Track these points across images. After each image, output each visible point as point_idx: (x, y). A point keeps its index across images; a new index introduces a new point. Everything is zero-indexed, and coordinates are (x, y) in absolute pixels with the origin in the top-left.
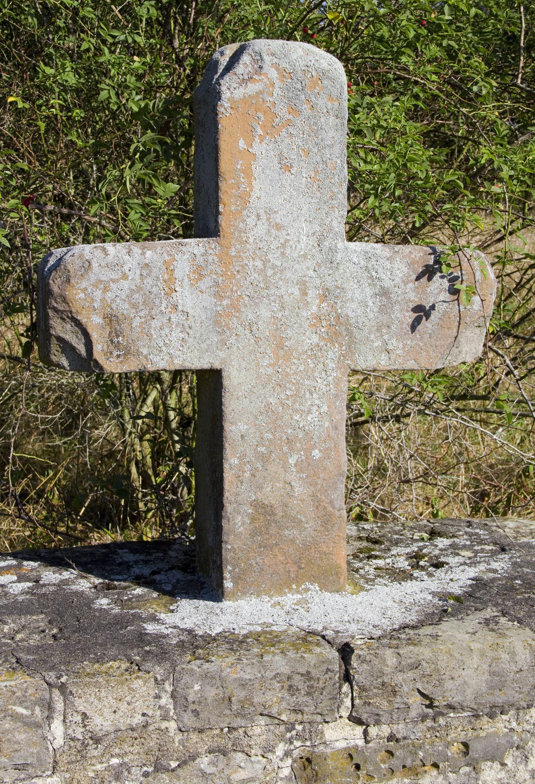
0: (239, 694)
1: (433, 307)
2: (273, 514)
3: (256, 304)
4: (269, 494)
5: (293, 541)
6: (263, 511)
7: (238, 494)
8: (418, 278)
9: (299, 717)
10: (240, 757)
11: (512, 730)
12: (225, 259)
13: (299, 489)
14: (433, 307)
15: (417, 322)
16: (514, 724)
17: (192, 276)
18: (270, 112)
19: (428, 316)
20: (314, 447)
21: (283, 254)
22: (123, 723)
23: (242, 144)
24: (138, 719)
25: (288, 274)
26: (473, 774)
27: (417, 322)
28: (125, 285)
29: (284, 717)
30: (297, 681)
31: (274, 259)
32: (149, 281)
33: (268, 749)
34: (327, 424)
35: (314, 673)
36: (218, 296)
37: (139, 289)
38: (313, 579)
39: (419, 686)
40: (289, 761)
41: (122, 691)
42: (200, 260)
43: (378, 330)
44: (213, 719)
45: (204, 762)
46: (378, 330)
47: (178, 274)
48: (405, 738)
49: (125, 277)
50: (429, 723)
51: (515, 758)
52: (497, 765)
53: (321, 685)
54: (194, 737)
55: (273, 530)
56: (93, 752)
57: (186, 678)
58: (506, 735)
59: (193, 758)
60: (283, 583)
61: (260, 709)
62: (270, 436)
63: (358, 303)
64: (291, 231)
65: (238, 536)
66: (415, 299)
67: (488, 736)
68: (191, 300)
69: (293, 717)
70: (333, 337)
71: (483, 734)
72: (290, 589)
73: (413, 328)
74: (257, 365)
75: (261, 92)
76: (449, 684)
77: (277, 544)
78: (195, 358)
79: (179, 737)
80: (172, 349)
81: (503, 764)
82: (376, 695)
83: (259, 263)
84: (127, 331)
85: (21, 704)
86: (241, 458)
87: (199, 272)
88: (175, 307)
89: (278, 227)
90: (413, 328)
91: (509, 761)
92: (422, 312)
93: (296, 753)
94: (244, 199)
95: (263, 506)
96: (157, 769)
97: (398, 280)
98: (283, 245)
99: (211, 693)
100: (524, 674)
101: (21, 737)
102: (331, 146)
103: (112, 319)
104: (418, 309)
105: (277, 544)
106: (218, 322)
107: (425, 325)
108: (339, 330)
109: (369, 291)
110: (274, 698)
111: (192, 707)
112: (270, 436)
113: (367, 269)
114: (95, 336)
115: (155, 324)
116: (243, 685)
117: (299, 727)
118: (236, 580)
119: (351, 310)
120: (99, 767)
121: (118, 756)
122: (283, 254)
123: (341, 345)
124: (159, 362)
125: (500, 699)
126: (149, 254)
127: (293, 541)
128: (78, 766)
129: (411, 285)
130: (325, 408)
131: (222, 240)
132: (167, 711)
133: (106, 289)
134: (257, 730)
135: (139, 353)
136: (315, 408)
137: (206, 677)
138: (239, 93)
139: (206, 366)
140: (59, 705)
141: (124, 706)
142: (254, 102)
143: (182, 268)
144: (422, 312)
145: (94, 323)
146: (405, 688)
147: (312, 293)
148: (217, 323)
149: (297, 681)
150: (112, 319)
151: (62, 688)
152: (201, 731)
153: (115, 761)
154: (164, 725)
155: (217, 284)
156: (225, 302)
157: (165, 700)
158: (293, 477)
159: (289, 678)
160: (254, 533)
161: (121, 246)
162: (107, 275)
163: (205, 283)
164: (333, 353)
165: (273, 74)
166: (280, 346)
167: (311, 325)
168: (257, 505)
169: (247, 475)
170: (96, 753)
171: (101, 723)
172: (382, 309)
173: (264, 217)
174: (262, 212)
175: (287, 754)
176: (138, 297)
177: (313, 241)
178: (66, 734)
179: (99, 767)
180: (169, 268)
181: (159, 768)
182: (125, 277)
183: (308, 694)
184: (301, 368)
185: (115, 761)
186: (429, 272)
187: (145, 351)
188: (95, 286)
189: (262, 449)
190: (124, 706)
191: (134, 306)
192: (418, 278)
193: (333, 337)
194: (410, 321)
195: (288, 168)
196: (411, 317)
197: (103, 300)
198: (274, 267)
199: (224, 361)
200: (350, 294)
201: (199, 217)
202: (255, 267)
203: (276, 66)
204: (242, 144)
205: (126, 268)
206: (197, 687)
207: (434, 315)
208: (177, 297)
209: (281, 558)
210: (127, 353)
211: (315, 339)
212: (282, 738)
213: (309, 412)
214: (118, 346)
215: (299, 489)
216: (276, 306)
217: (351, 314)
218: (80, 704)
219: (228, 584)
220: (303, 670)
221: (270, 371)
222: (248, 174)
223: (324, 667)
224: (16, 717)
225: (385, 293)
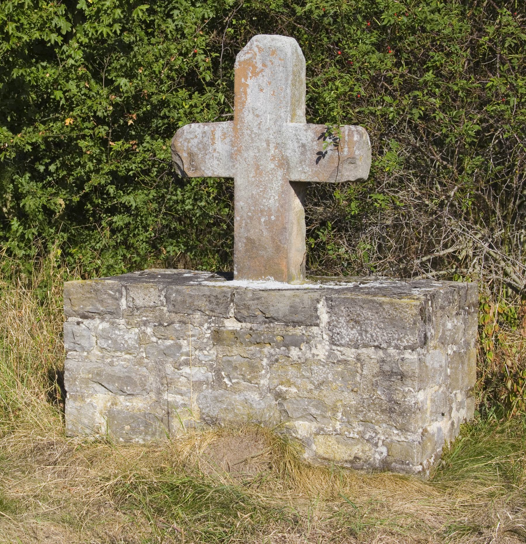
0: (189, 300)
1: (326, 152)
2: (254, 243)
3: (248, 150)
4: (253, 234)
5: (263, 256)
6: (250, 241)
7: (239, 233)
8: (319, 139)
9: (214, 314)
10: (190, 326)
11: (303, 334)
12: (235, 129)
13: (265, 233)
14: (326, 152)
15: (318, 159)
16: (304, 332)
17: (222, 137)
18: (254, 67)
19: (324, 156)
20: (272, 215)
21: (259, 128)
22: (146, 304)
23: (243, 80)
24: (152, 304)
25: (261, 137)
26: (287, 351)
27: (318, 159)
28: (196, 140)
29: (207, 313)
30: (212, 298)
31: (255, 130)
32: (205, 139)
33: (201, 325)
34: (278, 205)
35: (219, 296)
36: (232, 146)
37: (202, 142)
38: (272, 275)
39: (259, 307)
40: (209, 331)
41: (146, 292)
42: (225, 130)
43: (300, 163)
44: (180, 309)
45: (177, 326)
46: (300, 163)
47: (216, 136)
48: (257, 330)
49: (196, 137)
50: (267, 325)
51: (306, 347)
52: (297, 349)
53: (221, 301)
54: (173, 315)
55: (255, 251)
56: (136, 313)
57: (170, 291)
58: (300, 336)
59: (173, 323)
60: (258, 275)
61: (197, 308)
62: (253, 208)
63: (292, 152)
64: (263, 118)
65: (240, 251)
66: (317, 149)
67: (293, 335)
68: (221, 147)
69: (211, 313)
70: (281, 165)
71: (290, 334)
72: (262, 278)
73: (317, 162)
74: (248, 176)
75: (251, 58)
76: (271, 308)
77: (256, 257)
78: (223, 173)
79: (167, 314)
80: (214, 168)
81: (301, 349)
82: (242, 309)
83: (249, 132)
84: (196, 160)
85: (111, 290)
86: (241, 217)
87: (224, 135)
88: (215, 150)
89: (258, 116)
90: (317, 162)
91: (303, 348)
92: (321, 155)
93: (212, 328)
94: (243, 103)
95: (251, 239)
96: (159, 325)
97: (309, 140)
98: (259, 124)
99: (179, 298)
100: (306, 309)
101: (110, 301)
102: (280, 80)
103: (191, 155)
104: (319, 153)
105: (256, 257)
106: (232, 157)
107: (323, 161)
108: (284, 163)
109: (296, 145)
110: (203, 304)
111: (172, 303)
112: (253, 208)
113: (295, 135)
114: (184, 161)
115: (207, 157)
116: (191, 296)
117: (213, 318)
118: (239, 271)
119: (289, 153)
120: (138, 319)
121: (145, 316)
122: (259, 128)
123: (284, 169)
124: (208, 173)
125: (296, 318)
126: (206, 127)
127: (263, 256)
128: (131, 317)
129: (315, 143)
130: (277, 198)
131: (234, 121)
132: (163, 302)
133: (189, 142)
134: (197, 316)
135: (201, 169)
136: (272, 197)
137: (177, 291)
138: (242, 59)
139: (228, 176)
140: (124, 293)
141: (147, 298)
142: (249, 62)
143: (218, 134)
144: (321, 155)
145: (184, 155)
146: (253, 307)
147: (272, 146)
148: (232, 157)
149: (212, 298)
150: (191, 155)
151: (126, 287)
152: (176, 313)
153: (144, 318)
154: (162, 308)
155: (231, 141)
156: (235, 149)
157: (162, 298)
158: (263, 227)
159: (209, 297)
160: (247, 251)
161: (197, 125)
162: (189, 136)
163: (227, 140)
164: (280, 173)
165: (256, 50)
166: (258, 168)
167: (271, 160)
168: (247, 238)
169: (244, 225)
170: (137, 314)
171: (139, 302)
172: (303, 153)
173: (251, 112)
174: (250, 109)
175: (209, 328)
176: (203, 147)
177: (272, 122)
178: (127, 305)
179: (138, 319)
180: (213, 133)
181: (161, 324)
182: (196, 137)
183: (217, 305)
184: (267, 179)
185: (144, 318)
186: (322, 137)
187: (203, 169)
188: (185, 140)
189: (250, 214)
190: (147, 298)
191: (199, 149)
192: (319, 139)
193: (281, 165)
194: (315, 159)
195: (261, 90)
196: (315, 157)
197: (187, 146)
198: (255, 133)
199: (234, 174)
200: (288, 146)
201: (225, 111)
202: (247, 134)
203: (257, 46)
204: (243, 80)
205: (196, 133)
206: (174, 295)
207: (327, 156)
208: (215, 146)
209: (258, 263)
210: (196, 169)
211: (273, 166)
212: (206, 321)
213: (270, 199)
214: (193, 166)
215: (265, 233)
216: (256, 151)
217: (288, 155)
218: (132, 294)
219: (235, 273)
220: (215, 294)
221: (253, 179)
222: (246, 93)
223: (223, 294)
224: (110, 295)
225: (303, 146)
